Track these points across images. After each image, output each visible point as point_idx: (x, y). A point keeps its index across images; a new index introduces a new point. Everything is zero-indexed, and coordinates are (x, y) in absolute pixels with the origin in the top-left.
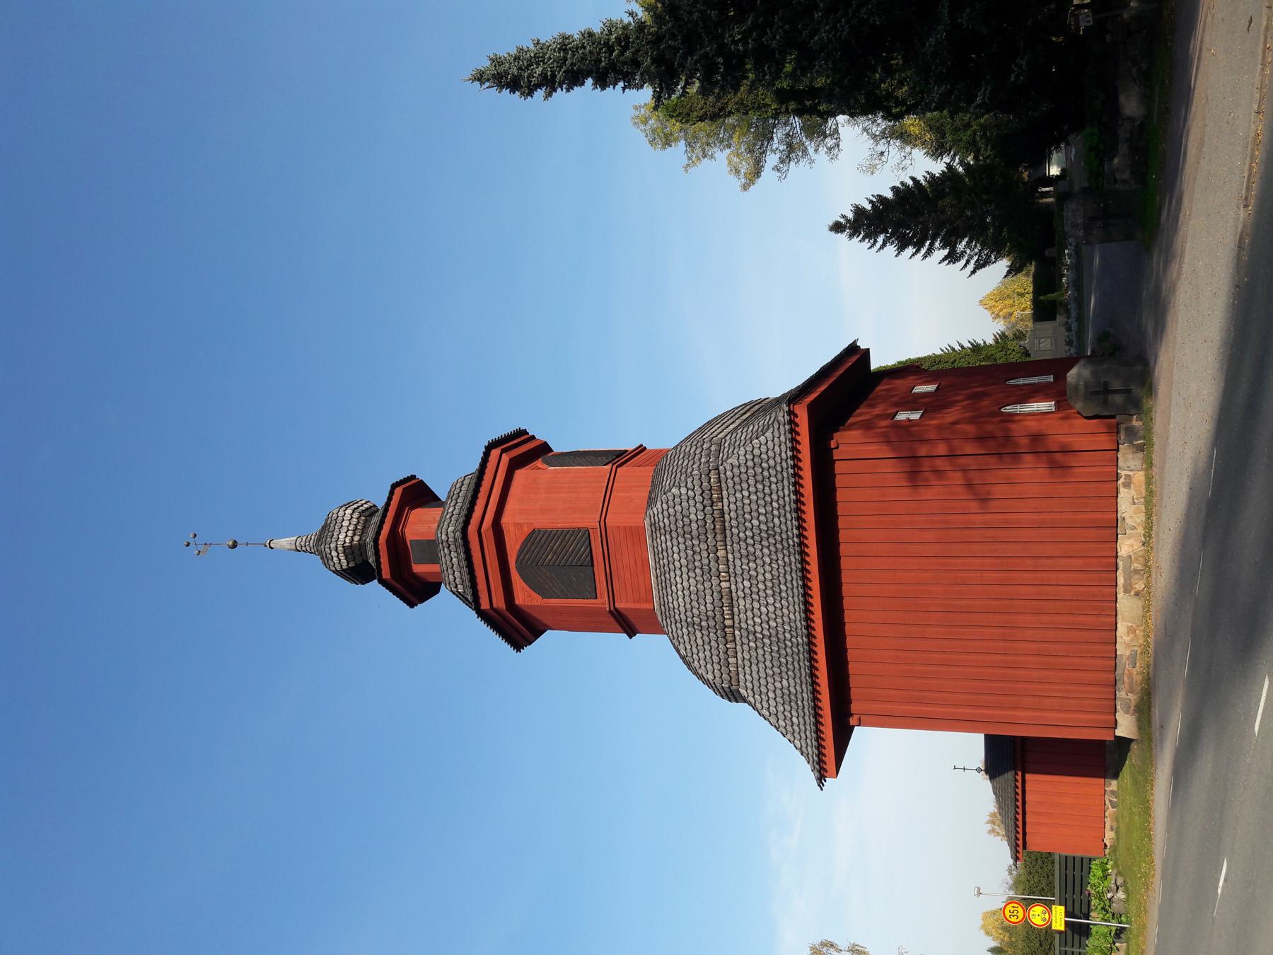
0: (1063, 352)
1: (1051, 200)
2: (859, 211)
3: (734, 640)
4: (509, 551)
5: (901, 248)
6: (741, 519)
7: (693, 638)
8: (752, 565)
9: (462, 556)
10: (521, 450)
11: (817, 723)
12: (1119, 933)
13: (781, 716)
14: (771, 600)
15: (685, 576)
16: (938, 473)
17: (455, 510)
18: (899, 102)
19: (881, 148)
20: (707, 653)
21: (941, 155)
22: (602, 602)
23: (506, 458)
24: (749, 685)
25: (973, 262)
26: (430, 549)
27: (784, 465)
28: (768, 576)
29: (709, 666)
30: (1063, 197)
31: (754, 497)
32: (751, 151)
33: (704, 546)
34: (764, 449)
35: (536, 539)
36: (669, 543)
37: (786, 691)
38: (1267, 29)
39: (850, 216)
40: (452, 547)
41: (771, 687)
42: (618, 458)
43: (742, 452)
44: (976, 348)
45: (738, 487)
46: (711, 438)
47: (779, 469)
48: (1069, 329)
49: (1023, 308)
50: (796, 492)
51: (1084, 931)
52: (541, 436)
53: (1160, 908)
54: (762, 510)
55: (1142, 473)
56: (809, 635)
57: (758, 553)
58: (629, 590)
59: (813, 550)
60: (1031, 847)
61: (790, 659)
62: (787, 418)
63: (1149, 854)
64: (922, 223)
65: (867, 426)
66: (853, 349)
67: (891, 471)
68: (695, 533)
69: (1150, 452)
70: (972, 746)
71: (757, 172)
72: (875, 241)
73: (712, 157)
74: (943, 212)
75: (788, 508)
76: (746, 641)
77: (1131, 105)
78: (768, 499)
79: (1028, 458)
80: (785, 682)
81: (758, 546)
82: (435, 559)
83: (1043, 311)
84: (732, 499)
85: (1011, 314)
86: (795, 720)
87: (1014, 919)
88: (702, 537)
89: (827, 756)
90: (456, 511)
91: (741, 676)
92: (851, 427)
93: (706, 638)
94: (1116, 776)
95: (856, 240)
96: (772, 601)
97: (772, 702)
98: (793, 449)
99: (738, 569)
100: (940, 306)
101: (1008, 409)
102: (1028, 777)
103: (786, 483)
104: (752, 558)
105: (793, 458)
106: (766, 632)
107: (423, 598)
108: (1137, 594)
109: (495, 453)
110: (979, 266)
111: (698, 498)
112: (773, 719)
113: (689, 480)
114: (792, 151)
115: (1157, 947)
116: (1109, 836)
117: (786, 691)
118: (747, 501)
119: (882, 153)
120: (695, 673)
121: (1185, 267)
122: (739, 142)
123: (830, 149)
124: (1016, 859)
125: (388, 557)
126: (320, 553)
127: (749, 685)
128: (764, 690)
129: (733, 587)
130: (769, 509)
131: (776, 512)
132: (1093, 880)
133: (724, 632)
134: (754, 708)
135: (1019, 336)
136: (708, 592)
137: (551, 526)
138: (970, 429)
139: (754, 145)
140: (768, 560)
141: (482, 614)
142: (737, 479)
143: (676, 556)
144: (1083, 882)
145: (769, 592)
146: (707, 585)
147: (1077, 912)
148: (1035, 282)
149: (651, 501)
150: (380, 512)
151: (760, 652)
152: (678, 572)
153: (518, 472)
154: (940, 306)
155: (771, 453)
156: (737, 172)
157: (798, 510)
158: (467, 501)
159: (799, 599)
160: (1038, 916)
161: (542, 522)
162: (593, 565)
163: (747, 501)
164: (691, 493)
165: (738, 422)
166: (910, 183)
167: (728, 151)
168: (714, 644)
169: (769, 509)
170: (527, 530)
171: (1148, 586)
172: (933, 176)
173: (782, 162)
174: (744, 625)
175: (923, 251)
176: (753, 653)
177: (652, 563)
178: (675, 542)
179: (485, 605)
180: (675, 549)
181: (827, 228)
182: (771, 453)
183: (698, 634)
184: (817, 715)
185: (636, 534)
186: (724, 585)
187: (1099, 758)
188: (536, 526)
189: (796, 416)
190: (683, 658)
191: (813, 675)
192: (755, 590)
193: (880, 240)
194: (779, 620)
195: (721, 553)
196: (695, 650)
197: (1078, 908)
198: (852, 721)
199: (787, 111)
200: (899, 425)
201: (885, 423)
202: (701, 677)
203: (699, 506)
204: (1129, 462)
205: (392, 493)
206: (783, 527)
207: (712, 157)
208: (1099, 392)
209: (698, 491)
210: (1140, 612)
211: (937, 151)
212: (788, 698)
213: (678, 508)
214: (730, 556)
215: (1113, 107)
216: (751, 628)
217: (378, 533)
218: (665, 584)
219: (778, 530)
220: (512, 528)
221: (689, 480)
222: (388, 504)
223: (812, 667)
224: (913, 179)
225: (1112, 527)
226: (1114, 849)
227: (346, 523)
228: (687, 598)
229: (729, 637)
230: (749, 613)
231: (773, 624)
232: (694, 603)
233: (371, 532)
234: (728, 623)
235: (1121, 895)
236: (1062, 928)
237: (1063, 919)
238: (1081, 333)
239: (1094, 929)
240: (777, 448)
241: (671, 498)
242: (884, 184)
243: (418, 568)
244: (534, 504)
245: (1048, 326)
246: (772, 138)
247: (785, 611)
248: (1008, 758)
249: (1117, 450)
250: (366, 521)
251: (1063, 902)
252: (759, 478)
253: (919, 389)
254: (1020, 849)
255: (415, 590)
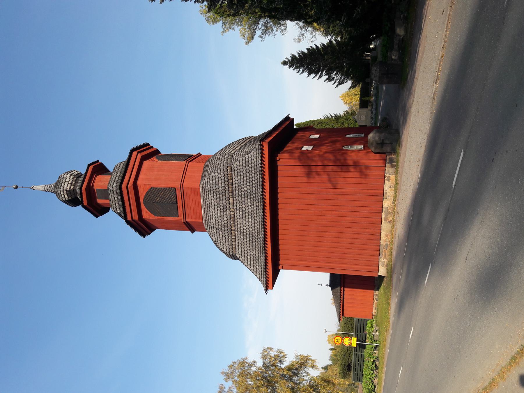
0: (368, 124)
1: (370, 58)
2: (293, 57)
3: (235, 235)
4: (140, 194)
5: (309, 74)
6: (240, 187)
7: (218, 234)
8: (243, 206)
9: (119, 197)
10: (146, 152)
11: (266, 268)
12: (376, 347)
13: (252, 265)
14: (250, 220)
15: (216, 209)
16: (318, 174)
17: (116, 177)
18: (310, 17)
19: (303, 32)
20: (224, 240)
21: (327, 35)
22: (181, 218)
23: (139, 156)
24: (240, 253)
25: (337, 82)
26: (105, 193)
27: (258, 166)
28: (250, 210)
29: (224, 246)
30: (374, 58)
31: (245, 179)
32: (250, 28)
33: (224, 197)
34: (250, 159)
35: (152, 191)
36: (210, 196)
37: (254, 256)
38: (449, 15)
39: (290, 58)
40: (115, 193)
41: (249, 254)
42: (189, 158)
43: (241, 160)
44: (337, 118)
45: (239, 174)
46: (229, 152)
47: (256, 168)
48: (372, 113)
49: (356, 100)
50: (262, 178)
51: (363, 347)
52: (156, 146)
53: (391, 339)
54: (248, 184)
55: (394, 176)
56: (265, 234)
57: (246, 201)
58: (192, 214)
59: (268, 201)
60: (345, 315)
61: (257, 243)
62: (260, 147)
63: (388, 319)
64: (318, 64)
65: (290, 152)
66: (287, 118)
67: (299, 170)
68: (221, 192)
69: (397, 168)
70: (325, 277)
71: (252, 37)
72: (299, 70)
73: (233, 29)
74: (327, 60)
75: (258, 184)
76: (239, 236)
77: (400, 31)
78: (251, 179)
79: (352, 169)
80: (254, 252)
81: (246, 198)
82: (107, 198)
83: (364, 104)
84: (236, 179)
85: (351, 103)
86: (257, 267)
87: (338, 343)
88: (224, 194)
89: (269, 280)
90: (117, 178)
91: (237, 250)
92: (283, 153)
93: (224, 234)
94: (378, 289)
95: (292, 69)
96: (251, 220)
97: (249, 260)
98: (262, 160)
99: (238, 207)
100: (323, 99)
101: (345, 148)
102: (345, 289)
103: (258, 173)
104: (243, 203)
105: (261, 164)
106: (248, 233)
107: (102, 214)
108: (389, 222)
109: (135, 153)
110: (339, 84)
111: (223, 178)
112: (249, 267)
113: (219, 170)
114: (267, 30)
115: (389, 354)
116: (375, 311)
117: (254, 256)
118: (242, 180)
119: (303, 35)
120: (219, 248)
121: (415, 99)
122: (246, 23)
123: (283, 31)
124: (340, 320)
125: (86, 195)
126: (56, 193)
127: (240, 253)
128: (246, 255)
129: (236, 214)
130: (251, 183)
131: (254, 185)
132: (368, 328)
133: (231, 232)
134: (242, 262)
135: (353, 113)
136: (225, 216)
137: (160, 186)
138: (331, 156)
139: (252, 26)
140: (250, 204)
141: (128, 222)
142: (238, 171)
143: (212, 201)
144: (364, 329)
145: (250, 217)
146: (225, 213)
147: (361, 340)
148: (361, 91)
149: (203, 178)
150: (83, 176)
151: (245, 240)
152: (213, 208)
153: (145, 162)
154: (323, 99)
155: (253, 161)
156: (244, 37)
157: (262, 185)
158: (122, 174)
159: (261, 220)
160: (346, 341)
161: (155, 184)
162: (177, 203)
163: (242, 180)
164: (219, 175)
165: (240, 146)
166: (315, 47)
167: (240, 27)
168: (227, 237)
169: (251, 183)
170: (148, 187)
171: (393, 219)
172: (324, 45)
173: (263, 34)
174: (239, 230)
175: (318, 76)
176: (242, 241)
177: (202, 203)
178: (212, 195)
179: (129, 218)
180: (212, 198)
181: (280, 63)
182: (253, 161)
183: (221, 233)
184: (266, 265)
185: (196, 191)
186: (232, 213)
187: (372, 283)
188: (152, 186)
189: (263, 146)
190: (214, 242)
191: (265, 250)
192: (244, 216)
193: (301, 70)
194: (253, 228)
195: (231, 200)
196: (219, 239)
197: (361, 339)
198: (280, 267)
199: (265, 16)
200: (303, 153)
201: (299, 151)
202: (221, 250)
203: (223, 181)
204: (389, 170)
205: (88, 168)
206: (256, 191)
207: (233, 29)
208: (382, 144)
209: (223, 175)
210: (390, 228)
211: (326, 33)
212: (255, 259)
213: (214, 181)
214: (235, 202)
215: (393, 30)
216: (242, 231)
217: (82, 186)
218: (207, 212)
219: (254, 192)
220: (142, 186)
221: (219, 170)
222: (86, 173)
223: (265, 247)
224: (315, 45)
225: (382, 196)
226: (376, 316)
227: (67, 180)
228: (216, 218)
229: (233, 234)
230: (241, 225)
231: (251, 229)
232: (219, 220)
233: (79, 184)
234: (233, 228)
235: (377, 333)
236: (355, 346)
237: (356, 342)
238: (376, 115)
239: (367, 346)
240: (255, 159)
241: (211, 177)
242: (304, 47)
243: (99, 201)
244: (152, 176)
245: (364, 110)
246: (259, 24)
247: (256, 224)
248: (338, 282)
249: (385, 166)
250: (76, 180)
251: (356, 336)
252: (248, 171)
253: (312, 137)
254: (341, 316)
255: (98, 210)
